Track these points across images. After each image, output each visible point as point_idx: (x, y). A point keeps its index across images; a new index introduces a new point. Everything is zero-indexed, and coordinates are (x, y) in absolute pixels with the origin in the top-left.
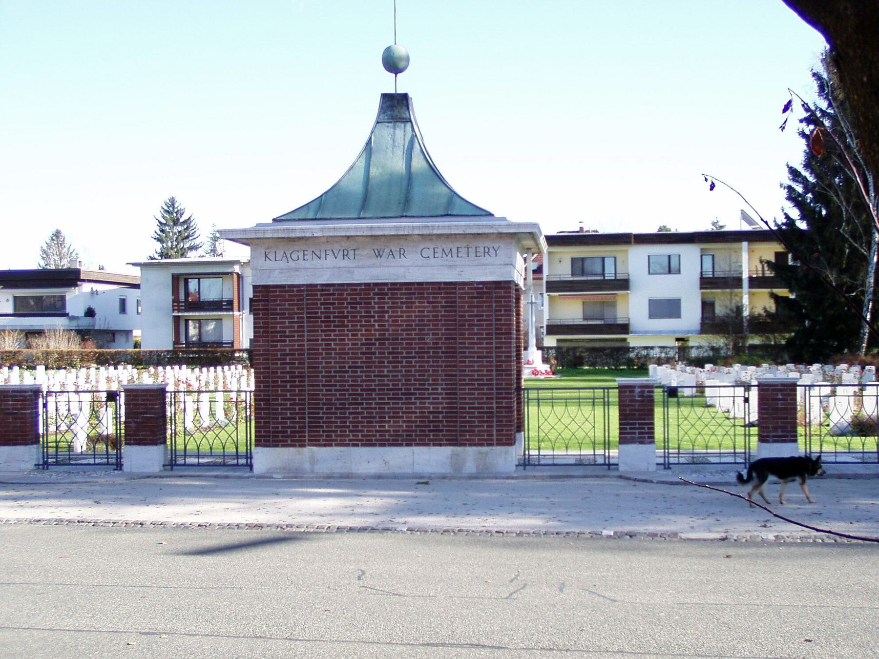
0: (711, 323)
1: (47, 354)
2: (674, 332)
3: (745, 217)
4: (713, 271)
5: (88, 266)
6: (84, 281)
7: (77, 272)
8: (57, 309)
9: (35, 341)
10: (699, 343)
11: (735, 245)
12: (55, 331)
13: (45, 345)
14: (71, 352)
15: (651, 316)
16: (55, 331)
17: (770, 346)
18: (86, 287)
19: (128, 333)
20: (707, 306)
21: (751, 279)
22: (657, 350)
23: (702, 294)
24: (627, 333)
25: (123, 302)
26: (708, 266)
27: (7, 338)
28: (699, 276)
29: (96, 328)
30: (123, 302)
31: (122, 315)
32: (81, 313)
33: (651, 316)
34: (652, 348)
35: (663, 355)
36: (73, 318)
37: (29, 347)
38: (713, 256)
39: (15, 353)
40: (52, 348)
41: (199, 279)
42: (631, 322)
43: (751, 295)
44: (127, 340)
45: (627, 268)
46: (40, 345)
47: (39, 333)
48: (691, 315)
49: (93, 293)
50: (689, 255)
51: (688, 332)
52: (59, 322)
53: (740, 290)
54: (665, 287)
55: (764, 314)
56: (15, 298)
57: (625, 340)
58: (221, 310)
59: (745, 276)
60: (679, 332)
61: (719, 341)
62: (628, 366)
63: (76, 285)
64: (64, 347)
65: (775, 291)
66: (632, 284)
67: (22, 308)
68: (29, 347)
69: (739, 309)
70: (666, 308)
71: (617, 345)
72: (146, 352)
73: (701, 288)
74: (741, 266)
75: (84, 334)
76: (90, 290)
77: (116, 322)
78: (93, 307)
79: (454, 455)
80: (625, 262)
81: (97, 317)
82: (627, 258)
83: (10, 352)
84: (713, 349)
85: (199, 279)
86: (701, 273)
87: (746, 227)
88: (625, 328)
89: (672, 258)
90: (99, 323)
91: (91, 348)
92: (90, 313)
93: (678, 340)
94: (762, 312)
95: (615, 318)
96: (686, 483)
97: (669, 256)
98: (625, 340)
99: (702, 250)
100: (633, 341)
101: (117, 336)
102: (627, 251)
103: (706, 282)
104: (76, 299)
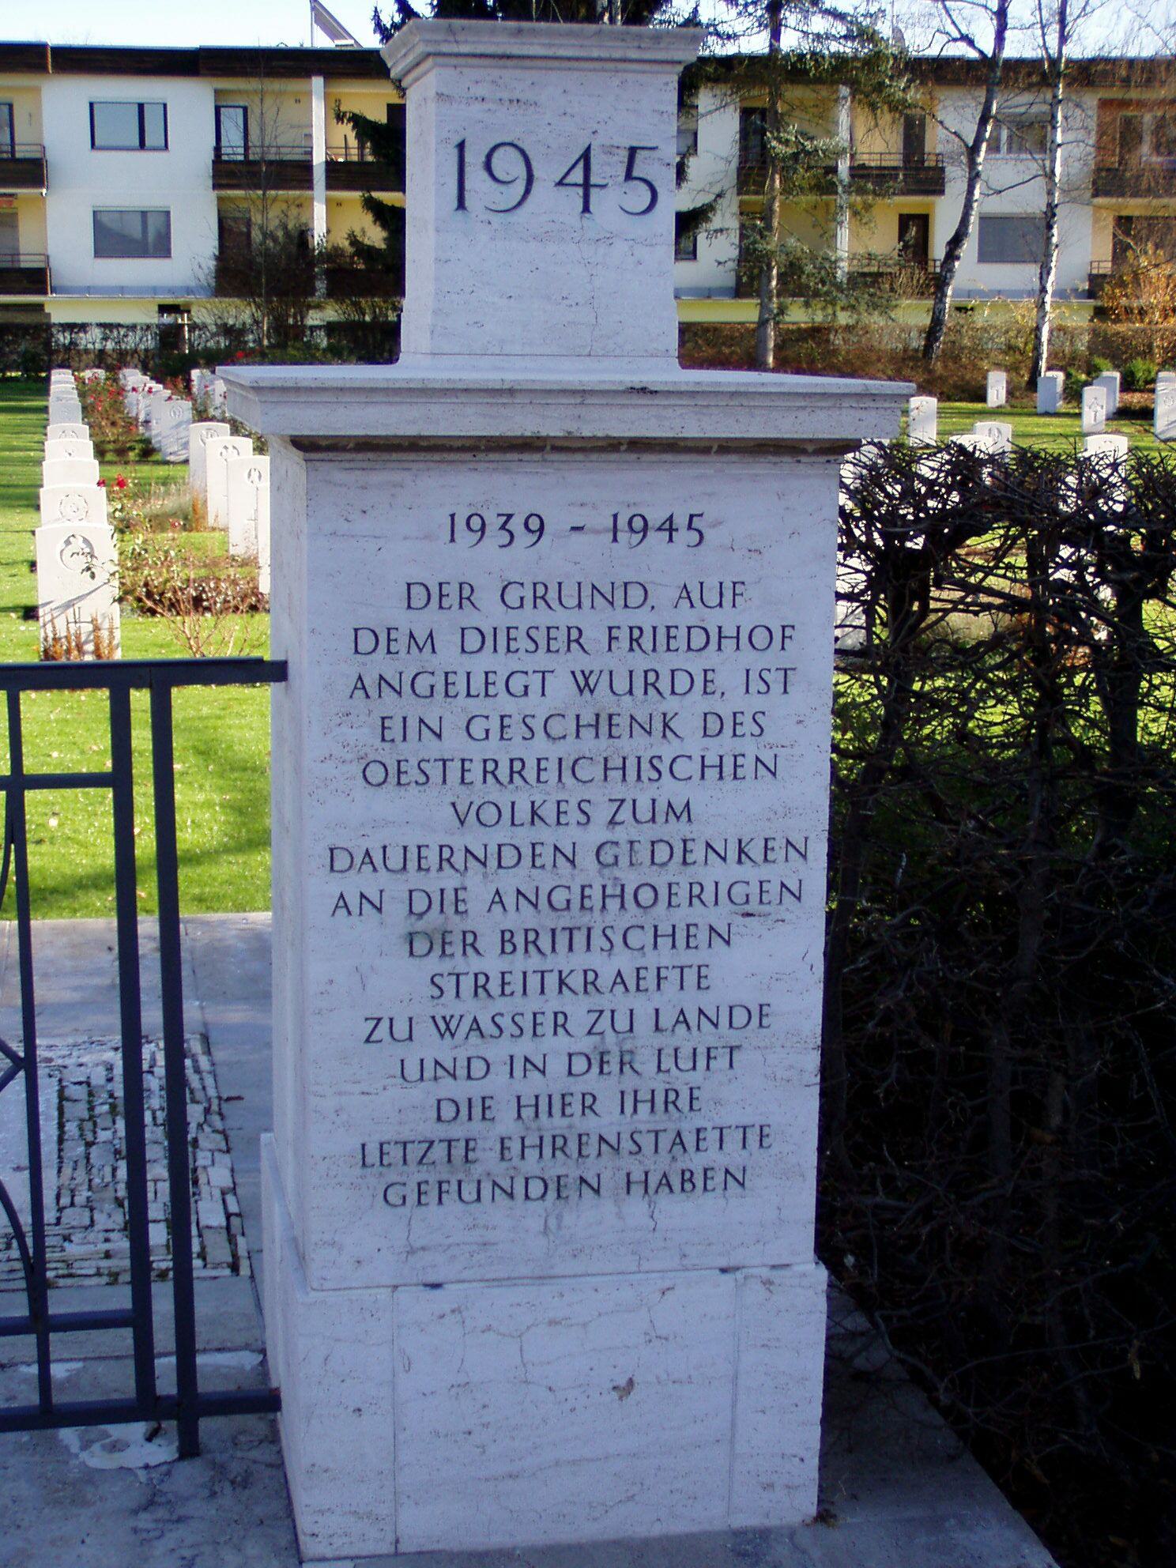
0: (236, 269)
2: (155, 290)
3: (323, 18)
4: (246, 148)
10: (208, 314)
11: (293, 85)
15: (99, 253)
17: (362, 325)
20: (230, 231)
21: (331, 166)
22: (97, 333)
23: (220, 199)
24: (45, 293)
26: (233, 138)
28: (211, 156)
33: (99, 253)
34: (83, 327)
35: (110, 345)
38: (245, 109)
42: (53, 263)
43: (332, 206)
45: (41, 133)
48: (195, 246)
50: (189, 104)
51: (189, 291)
53: (309, 193)
54: (129, 182)
55: (350, 250)
57: (39, 307)
58: (754, 363)
59: (319, 158)
60: (171, 291)
61: (240, 312)
62: (26, 370)
65: (376, 195)
66: (53, 173)
69: (303, 236)
70: (129, 235)
71: (21, 318)
73: (216, 186)
74: (309, 136)
80: (35, 117)
82: (39, 107)
84: (227, 330)
86: (218, 149)
87: (323, 41)
88: (37, 279)
89: (146, 108)
93: (163, 309)
94: (345, 244)
95: (16, 254)
96: (953, 23)
97: (141, 107)
98: (39, 307)
99: (217, 92)
100: (58, 310)
102: (37, 90)
103: (226, 173)
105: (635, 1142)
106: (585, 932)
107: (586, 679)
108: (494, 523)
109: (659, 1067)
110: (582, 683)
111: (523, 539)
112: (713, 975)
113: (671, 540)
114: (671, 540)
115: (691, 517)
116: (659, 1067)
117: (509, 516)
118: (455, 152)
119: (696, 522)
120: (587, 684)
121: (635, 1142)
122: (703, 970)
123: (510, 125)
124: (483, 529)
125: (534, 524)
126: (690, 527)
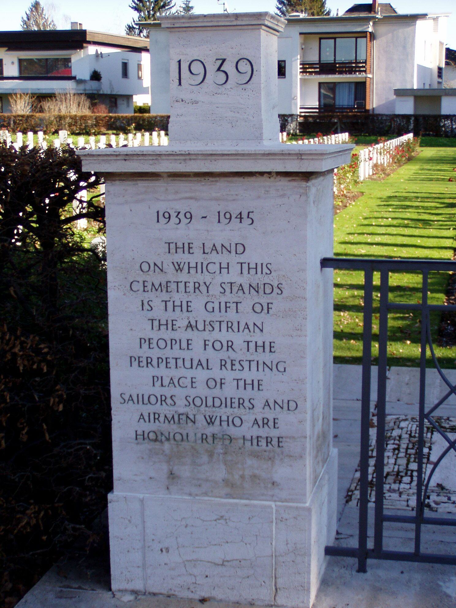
1: (60, 118)
5: (91, 26)
6: (89, 43)
7: (83, 33)
8: (58, 71)
9: (46, 105)
12: (65, 95)
13: (57, 109)
14: (85, 116)
16: (65, 95)
18: (92, 50)
19: (129, 97)
25: (125, 66)
27: (18, 101)
29: (101, 92)
30: (125, 66)
31: (125, 80)
32: (87, 77)
36: (80, 82)
37: (42, 110)
39: (28, 117)
40: (63, 112)
41: (356, 38)
44: (128, 105)
46: (52, 109)
47: (49, 96)
49: (98, 56)
52: (69, 85)
56: (20, 61)
63: (81, 47)
64: (74, 110)
67: (27, 72)
68: (42, 110)
72: (156, 117)
75: (94, 98)
76: (94, 53)
77: (120, 86)
78: (98, 70)
79: (165, 439)
81: (103, 80)
83: (23, 116)
85: (335, 39)
90: (105, 88)
91: (103, 112)
92: (96, 76)
101: (119, 102)
104: (81, 61)
105: (187, 401)
106: (182, 360)
107: (211, 419)
108: (173, 215)
109: (236, 252)
110: (209, 421)
111: (184, 221)
112: (280, 423)
113: (241, 222)
114: (241, 222)
115: (249, 213)
116: (236, 252)
117: (179, 213)
118: (178, 63)
119: (251, 215)
120: (211, 421)
121: (187, 401)
122: (272, 344)
123: (194, 53)
124: (169, 218)
125: (188, 215)
126: (248, 217)
